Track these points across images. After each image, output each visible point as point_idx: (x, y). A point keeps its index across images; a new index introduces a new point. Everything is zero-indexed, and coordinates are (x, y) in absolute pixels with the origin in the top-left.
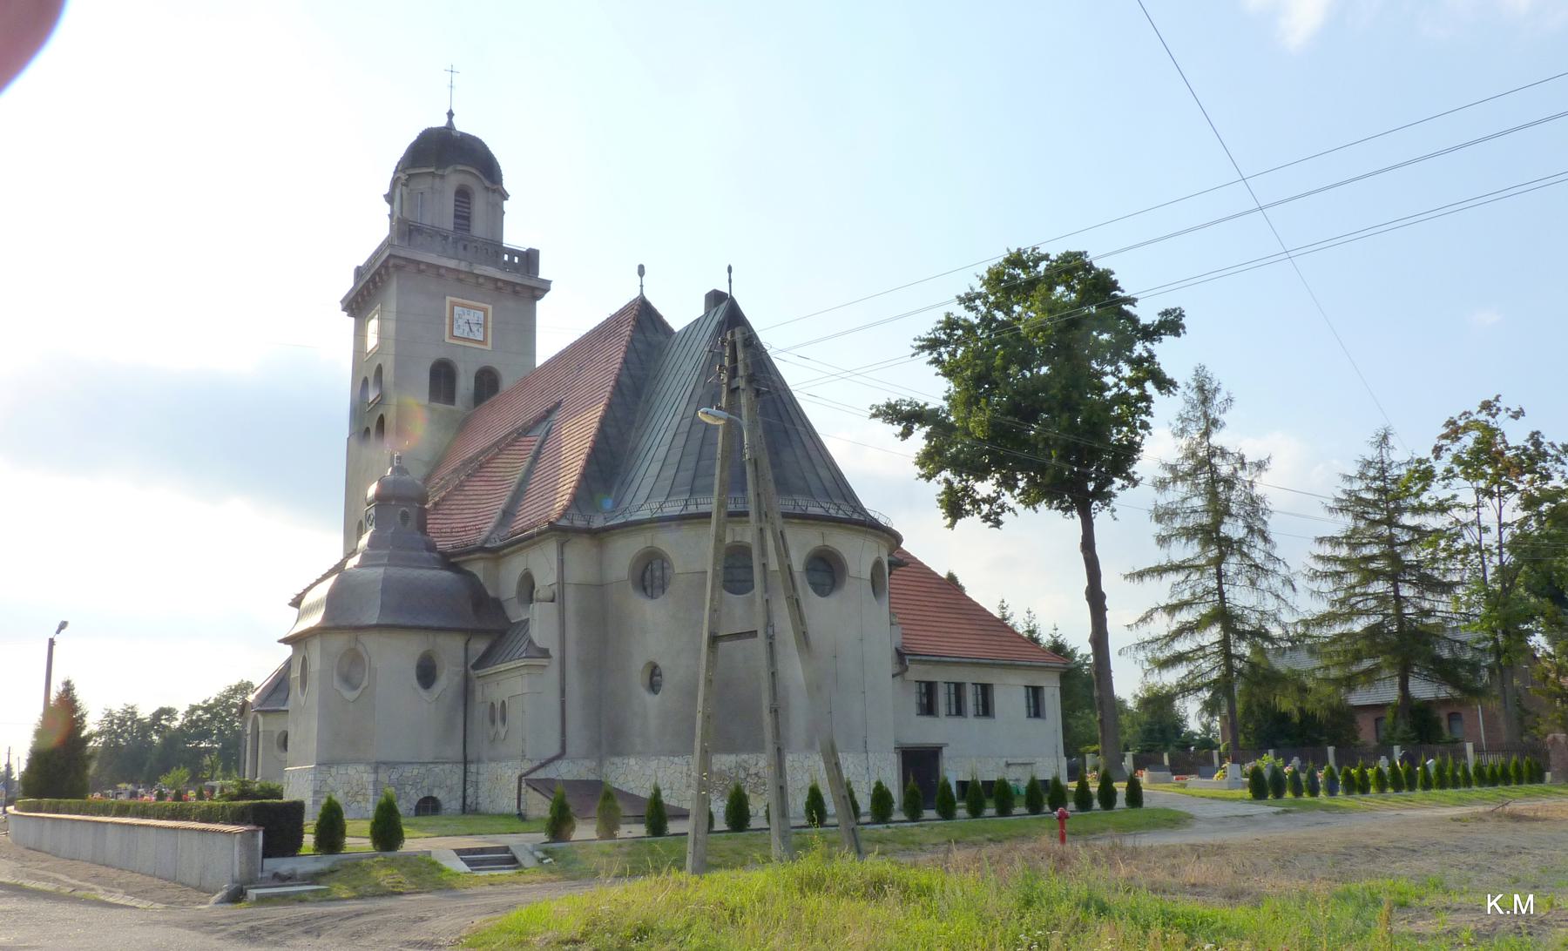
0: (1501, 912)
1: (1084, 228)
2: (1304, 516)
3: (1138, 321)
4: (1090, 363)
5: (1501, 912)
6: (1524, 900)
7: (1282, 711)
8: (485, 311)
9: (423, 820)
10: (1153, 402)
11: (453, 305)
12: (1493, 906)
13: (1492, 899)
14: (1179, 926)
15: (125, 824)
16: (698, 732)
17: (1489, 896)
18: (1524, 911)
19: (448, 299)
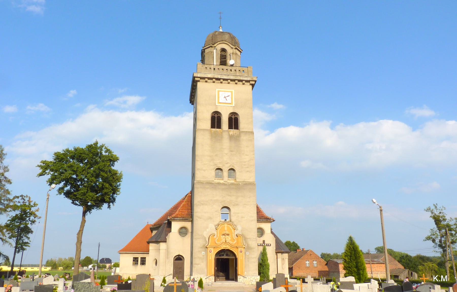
0: (437, 281)
3: (362, 251)
4: (12, 284)
8: (232, 92)
9: (5, 279)
10: (97, 143)
11: (219, 91)
13: (435, 277)
19: (217, 90)
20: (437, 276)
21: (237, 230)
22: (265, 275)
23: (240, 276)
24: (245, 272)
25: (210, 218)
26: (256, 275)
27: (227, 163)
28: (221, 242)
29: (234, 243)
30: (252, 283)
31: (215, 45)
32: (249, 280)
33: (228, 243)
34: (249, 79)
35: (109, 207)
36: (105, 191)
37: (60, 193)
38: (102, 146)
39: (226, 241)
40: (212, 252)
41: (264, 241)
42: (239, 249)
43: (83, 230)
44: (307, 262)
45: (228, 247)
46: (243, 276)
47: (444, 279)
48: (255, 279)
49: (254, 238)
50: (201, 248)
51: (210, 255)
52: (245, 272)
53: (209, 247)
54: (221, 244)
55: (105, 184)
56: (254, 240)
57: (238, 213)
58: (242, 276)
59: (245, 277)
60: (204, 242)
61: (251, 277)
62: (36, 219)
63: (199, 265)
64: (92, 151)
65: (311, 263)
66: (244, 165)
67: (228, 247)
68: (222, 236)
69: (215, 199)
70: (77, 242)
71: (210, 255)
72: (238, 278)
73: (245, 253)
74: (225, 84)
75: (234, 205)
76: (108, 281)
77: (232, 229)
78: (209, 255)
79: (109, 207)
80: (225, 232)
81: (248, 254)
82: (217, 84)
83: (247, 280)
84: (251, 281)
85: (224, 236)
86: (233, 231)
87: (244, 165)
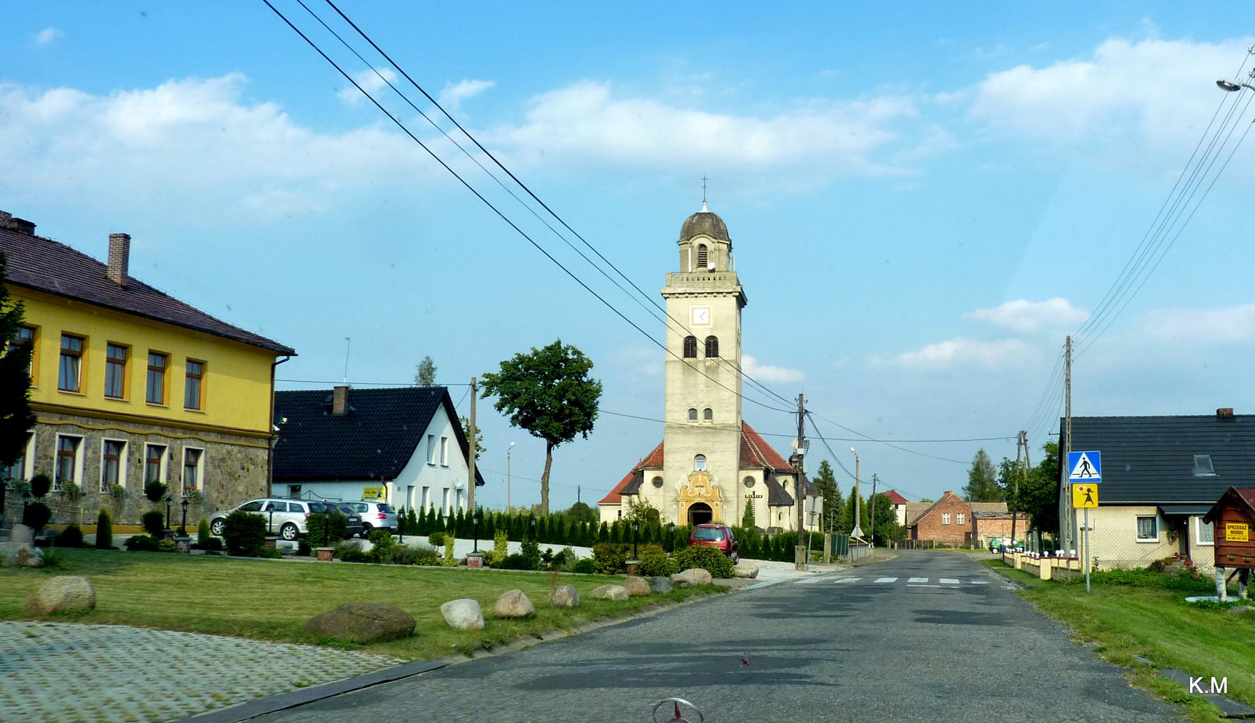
0: (1201, 692)
1: (520, 199)
5: (1201, 692)
6: (1219, 683)
7: (362, 551)
8: (709, 309)
10: (559, 343)
12: (1194, 687)
14: (600, 645)
17: (1191, 678)
18: (1219, 691)
25: (682, 468)
27: (702, 402)
28: (695, 495)
31: (691, 241)
34: (730, 291)
35: (585, 436)
36: (574, 418)
37: (514, 425)
38: (567, 349)
41: (754, 492)
43: (549, 472)
44: (946, 516)
45: (702, 501)
55: (573, 408)
57: (715, 462)
62: (479, 452)
64: (552, 362)
65: (954, 518)
66: (723, 403)
69: (688, 445)
70: (542, 490)
74: (701, 299)
75: (710, 453)
76: (330, 408)
79: (585, 436)
80: (698, 484)
82: (691, 299)
86: (708, 482)
87: (723, 403)
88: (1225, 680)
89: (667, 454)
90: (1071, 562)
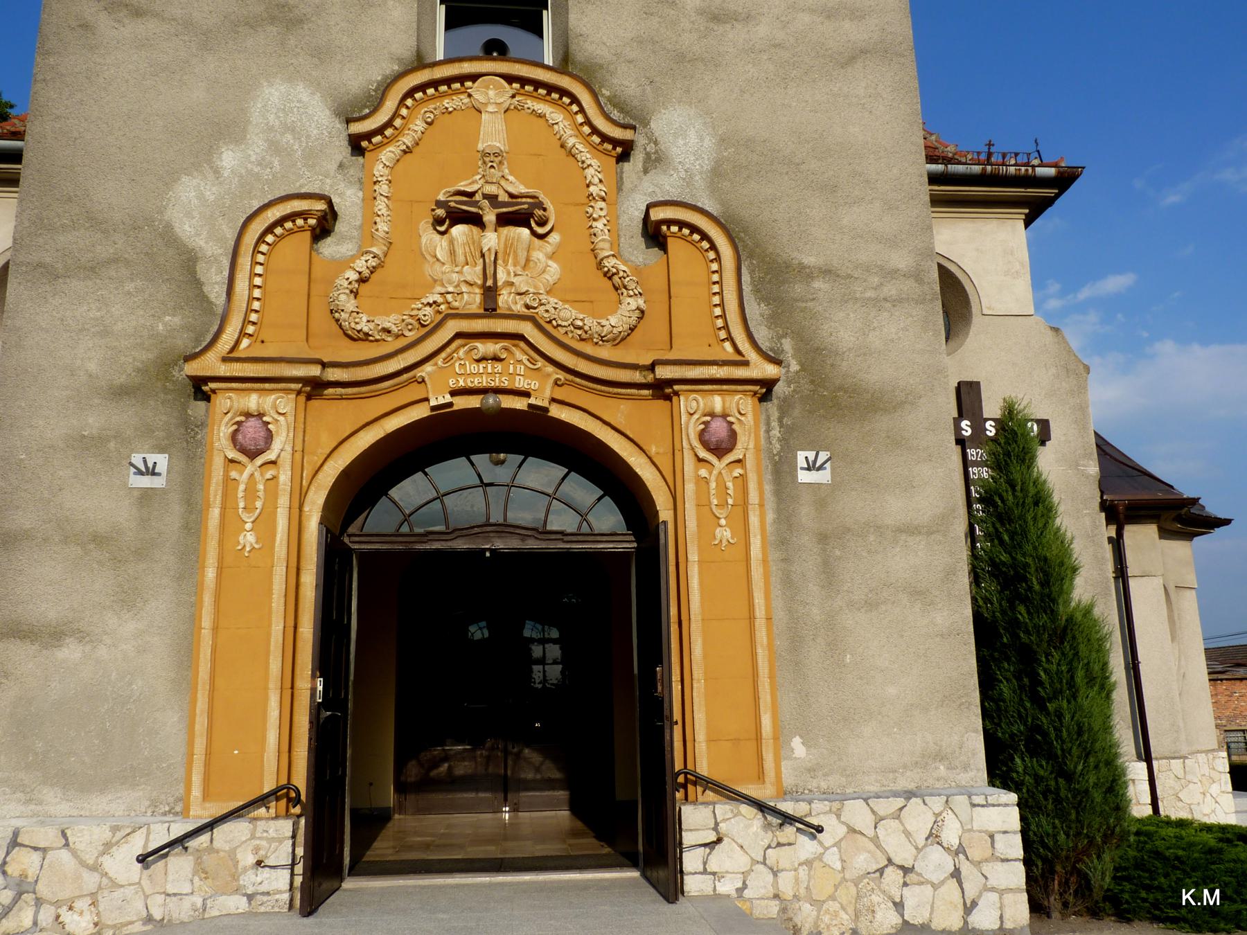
0: (1193, 904)
2: (304, 432)
5: (1193, 904)
12: (1187, 900)
13: (1186, 894)
15: (271, 583)
16: (208, 599)
17: (1184, 891)
20: (1193, 890)
21: (655, 161)
22: (1069, 777)
23: (724, 809)
24: (797, 742)
26: (964, 778)
29: (617, 321)
30: (899, 906)
32: (864, 861)
33: (527, 329)
39: (490, 292)
40: (280, 446)
42: (690, 404)
46: (761, 807)
47: (1212, 897)
48: (951, 835)
49: (893, 274)
50: (120, 393)
51: (251, 492)
52: (797, 742)
53: (224, 370)
54: (412, 335)
56: (890, 290)
58: (745, 809)
59: (787, 819)
60: (174, 320)
61: (887, 806)
63: (70, 652)
67: (521, 383)
68: (436, 244)
71: (251, 492)
72: (688, 838)
73: (781, 469)
77: (585, 154)
78: (229, 483)
81: (824, 477)
83: (833, 859)
84: (893, 875)
85: (459, 230)
86: (595, 166)
88: (1217, 892)
89: (577, 367)
90: (19, 840)
